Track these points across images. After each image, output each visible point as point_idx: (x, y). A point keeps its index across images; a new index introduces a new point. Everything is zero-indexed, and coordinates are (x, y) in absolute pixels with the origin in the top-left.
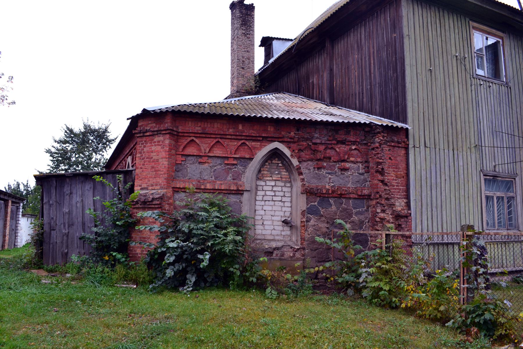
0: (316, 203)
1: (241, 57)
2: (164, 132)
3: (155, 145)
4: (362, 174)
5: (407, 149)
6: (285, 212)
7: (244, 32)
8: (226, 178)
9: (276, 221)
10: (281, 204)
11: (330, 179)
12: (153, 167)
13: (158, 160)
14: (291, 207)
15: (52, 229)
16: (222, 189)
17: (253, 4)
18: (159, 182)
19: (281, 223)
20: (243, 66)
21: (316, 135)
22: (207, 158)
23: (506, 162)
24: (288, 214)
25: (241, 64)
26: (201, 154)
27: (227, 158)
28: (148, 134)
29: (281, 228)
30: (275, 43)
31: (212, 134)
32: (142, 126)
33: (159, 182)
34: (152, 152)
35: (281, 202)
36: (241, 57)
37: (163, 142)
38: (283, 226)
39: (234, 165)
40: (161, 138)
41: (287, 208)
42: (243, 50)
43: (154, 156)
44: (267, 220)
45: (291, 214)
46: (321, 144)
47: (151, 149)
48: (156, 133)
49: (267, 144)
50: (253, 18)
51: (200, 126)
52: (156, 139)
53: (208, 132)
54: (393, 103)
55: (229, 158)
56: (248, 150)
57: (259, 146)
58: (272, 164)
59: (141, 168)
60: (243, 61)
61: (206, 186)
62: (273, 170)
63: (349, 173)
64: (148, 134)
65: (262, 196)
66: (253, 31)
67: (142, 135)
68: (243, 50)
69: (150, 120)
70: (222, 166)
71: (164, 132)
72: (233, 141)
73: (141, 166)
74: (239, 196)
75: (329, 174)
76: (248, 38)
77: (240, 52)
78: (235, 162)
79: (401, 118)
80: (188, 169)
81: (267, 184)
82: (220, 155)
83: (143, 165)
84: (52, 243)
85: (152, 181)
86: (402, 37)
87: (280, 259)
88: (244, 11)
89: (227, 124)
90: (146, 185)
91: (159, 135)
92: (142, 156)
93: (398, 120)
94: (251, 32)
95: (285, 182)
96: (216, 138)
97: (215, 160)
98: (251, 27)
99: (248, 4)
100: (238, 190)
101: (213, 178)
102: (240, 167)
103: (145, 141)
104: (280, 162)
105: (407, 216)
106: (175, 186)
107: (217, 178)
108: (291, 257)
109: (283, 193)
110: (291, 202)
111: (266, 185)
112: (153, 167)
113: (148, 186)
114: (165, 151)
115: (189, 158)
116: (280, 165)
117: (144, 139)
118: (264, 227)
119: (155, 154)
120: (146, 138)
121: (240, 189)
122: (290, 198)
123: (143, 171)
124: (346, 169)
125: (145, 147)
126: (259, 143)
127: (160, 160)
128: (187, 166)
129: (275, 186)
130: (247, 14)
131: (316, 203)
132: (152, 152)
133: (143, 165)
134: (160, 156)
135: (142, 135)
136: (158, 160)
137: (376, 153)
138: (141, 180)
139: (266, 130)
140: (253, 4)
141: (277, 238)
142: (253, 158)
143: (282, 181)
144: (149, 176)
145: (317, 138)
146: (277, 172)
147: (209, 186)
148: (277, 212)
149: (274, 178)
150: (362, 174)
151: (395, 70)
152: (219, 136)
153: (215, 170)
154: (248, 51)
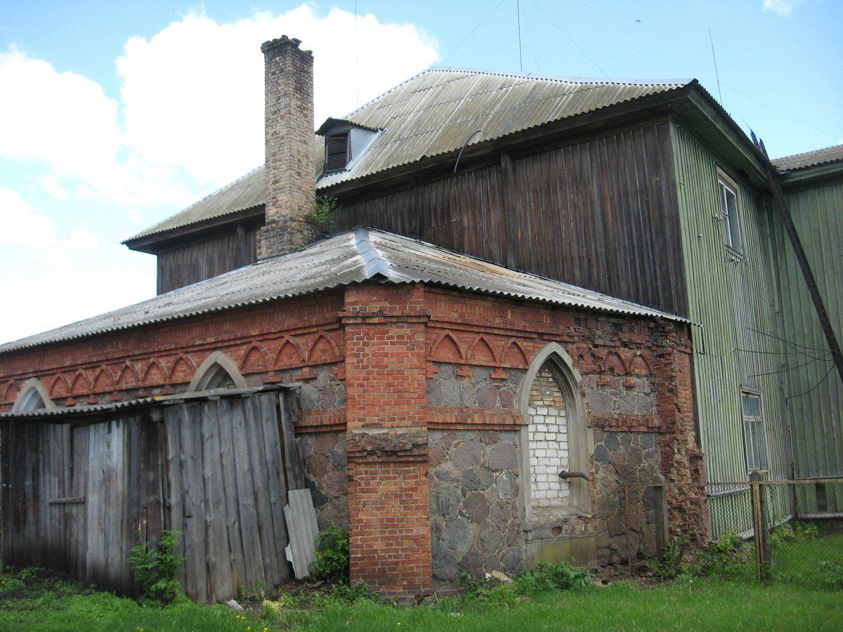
0: (603, 443)
1: (295, 152)
2: (415, 320)
3: (392, 343)
4: (647, 395)
5: (691, 355)
6: (561, 458)
7: (299, 103)
8: (494, 404)
9: (551, 474)
10: (555, 445)
11: (615, 402)
12: (389, 385)
13: (401, 372)
14: (568, 450)
15: (187, 514)
16: (496, 423)
17: (310, 52)
18: (408, 413)
19: (557, 478)
20: (299, 171)
21: (599, 333)
22: (468, 368)
23: (756, 377)
24: (565, 462)
25: (296, 166)
26: (461, 361)
27: (495, 368)
28: (376, 320)
29: (556, 486)
30: (354, 134)
31: (475, 326)
32: (355, 303)
33: (408, 413)
34: (386, 355)
35: (555, 443)
36: (295, 152)
37: (409, 338)
38: (560, 483)
39: (503, 380)
40: (406, 331)
41: (564, 452)
42: (298, 138)
43: (391, 363)
44: (541, 474)
45: (569, 462)
46: (604, 346)
47: (383, 349)
48: (395, 320)
49: (541, 346)
50: (311, 79)
51: (457, 311)
52: (393, 331)
53: (470, 323)
54: (659, 284)
55: (497, 370)
56: (518, 355)
57: (531, 349)
58: (542, 379)
59: (362, 385)
60: (299, 161)
61: (473, 419)
62: (543, 389)
63: (635, 393)
64: (376, 320)
65: (532, 434)
66: (312, 103)
67: (359, 321)
68: (298, 138)
69: (376, 295)
70: (487, 382)
71: (415, 320)
72: (500, 338)
73: (361, 381)
74: (512, 435)
75: (614, 394)
76: (306, 116)
77: (294, 141)
78: (504, 376)
79: (676, 309)
80: (442, 388)
81: (538, 413)
82: (485, 364)
83: (366, 379)
84: (190, 546)
85: (389, 411)
86: (672, 185)
87: (571, 538)
88: (299, 64)
89: (493, 310)
90: (376, 418)
91: (401, 324)
92: (362, 361)
93: (669, 309)
94: (309, 105)
95: (559, 409)
96: (479, 333)
97: (478, 370)
98: (308, 95)
99: (304, 50)
100: (515, 425)
101: (477, 404)
102: (511, 385)
103: (367, 334)
104: (550, 375)
105: (700, 458)
106: (432, 421)
107: (482, 403)
108: (583, 533)
109: (557, 426)
110: (568, 442)
111: (537, 415)
112: (389, 385)
113: (384, 420)
114: (418, 355)
115: (444, 368)
116: (551, 380)
117: (364, 328)
118: (537, 485)
119: (394, 359)
120: (368, 327)
121: (518, 422)
122: (566, 436)
123: (365, 391)
124: (630, 387)
125: (365, 344)
126: (531, 344)
127: (406, 373)
128: (440, 383)
129: (548, 415)
130: (303, 71)
131: (603, 443)
132: (386, 355)
133: (366, 379)
134: (406, 363)
135: (359, 321)
136: (401, 372)
137: (666, 362)
138: (363, 409)
139: (540, 322)
140: (310, 52)
141: (554, 503)
142: (527, 369)
143: (556, 407)
144: (382, 401)
145: (600, 337)
146: (548, 393)
147: (477, 420)
148: (552, 459)
149: (546, 403)
150: (647, 395)
151: (661, 232)
152: (483, 330)
153: (479, 389)
154: (305, 142)
